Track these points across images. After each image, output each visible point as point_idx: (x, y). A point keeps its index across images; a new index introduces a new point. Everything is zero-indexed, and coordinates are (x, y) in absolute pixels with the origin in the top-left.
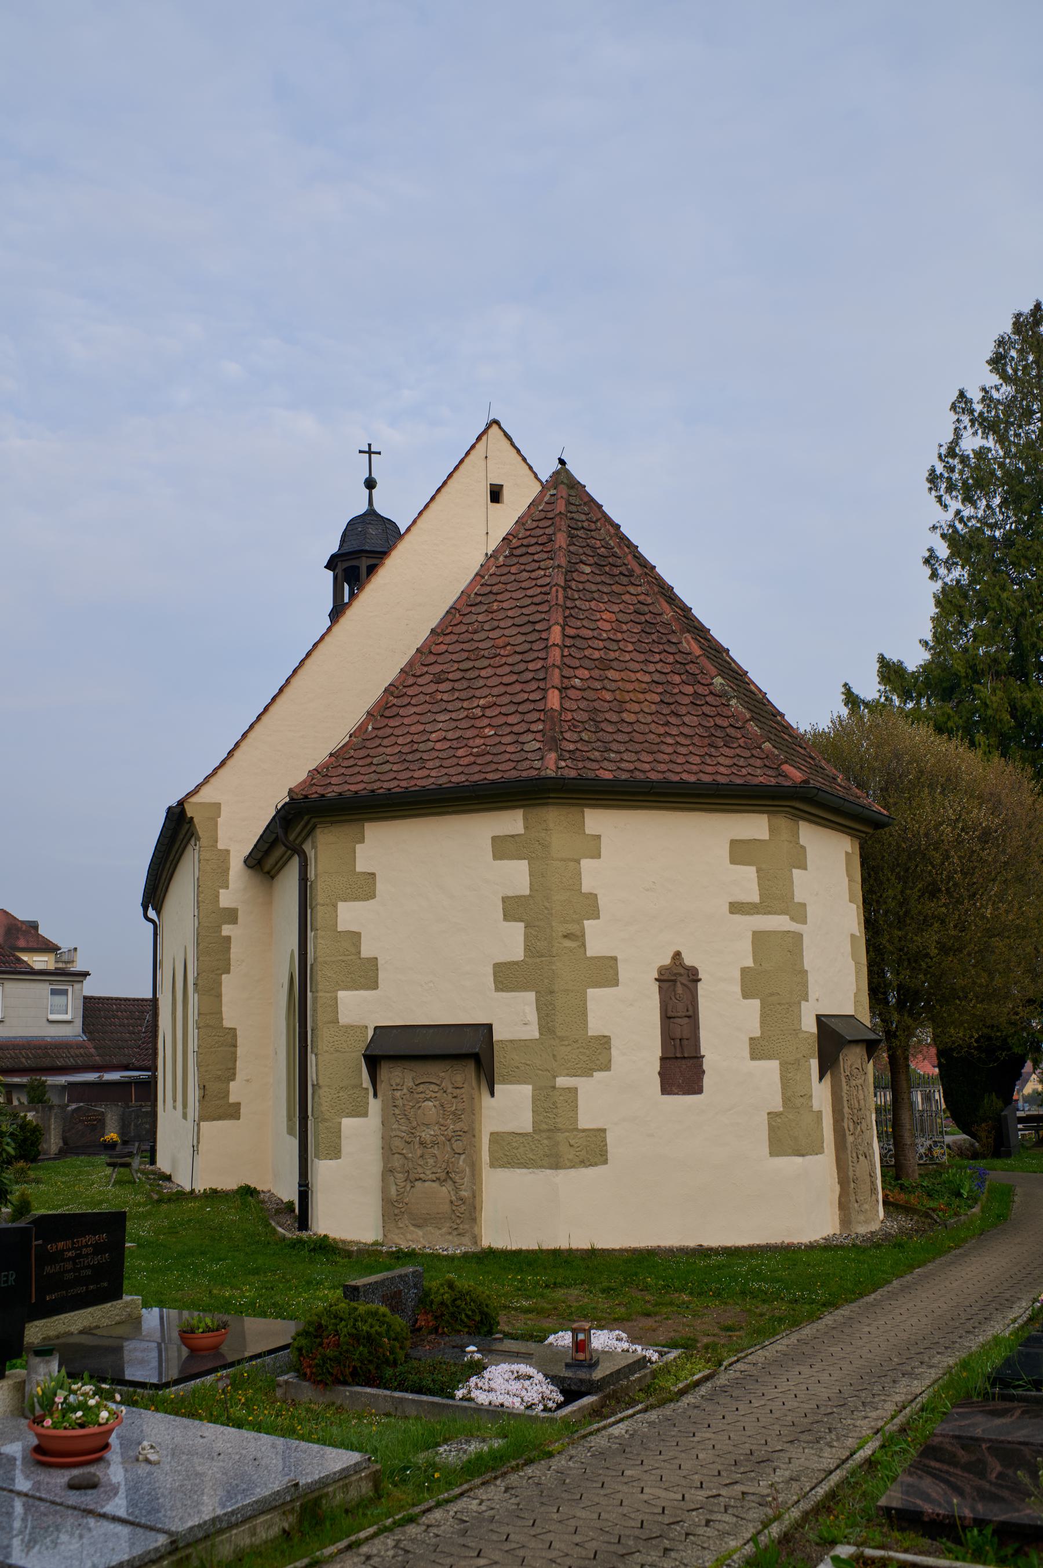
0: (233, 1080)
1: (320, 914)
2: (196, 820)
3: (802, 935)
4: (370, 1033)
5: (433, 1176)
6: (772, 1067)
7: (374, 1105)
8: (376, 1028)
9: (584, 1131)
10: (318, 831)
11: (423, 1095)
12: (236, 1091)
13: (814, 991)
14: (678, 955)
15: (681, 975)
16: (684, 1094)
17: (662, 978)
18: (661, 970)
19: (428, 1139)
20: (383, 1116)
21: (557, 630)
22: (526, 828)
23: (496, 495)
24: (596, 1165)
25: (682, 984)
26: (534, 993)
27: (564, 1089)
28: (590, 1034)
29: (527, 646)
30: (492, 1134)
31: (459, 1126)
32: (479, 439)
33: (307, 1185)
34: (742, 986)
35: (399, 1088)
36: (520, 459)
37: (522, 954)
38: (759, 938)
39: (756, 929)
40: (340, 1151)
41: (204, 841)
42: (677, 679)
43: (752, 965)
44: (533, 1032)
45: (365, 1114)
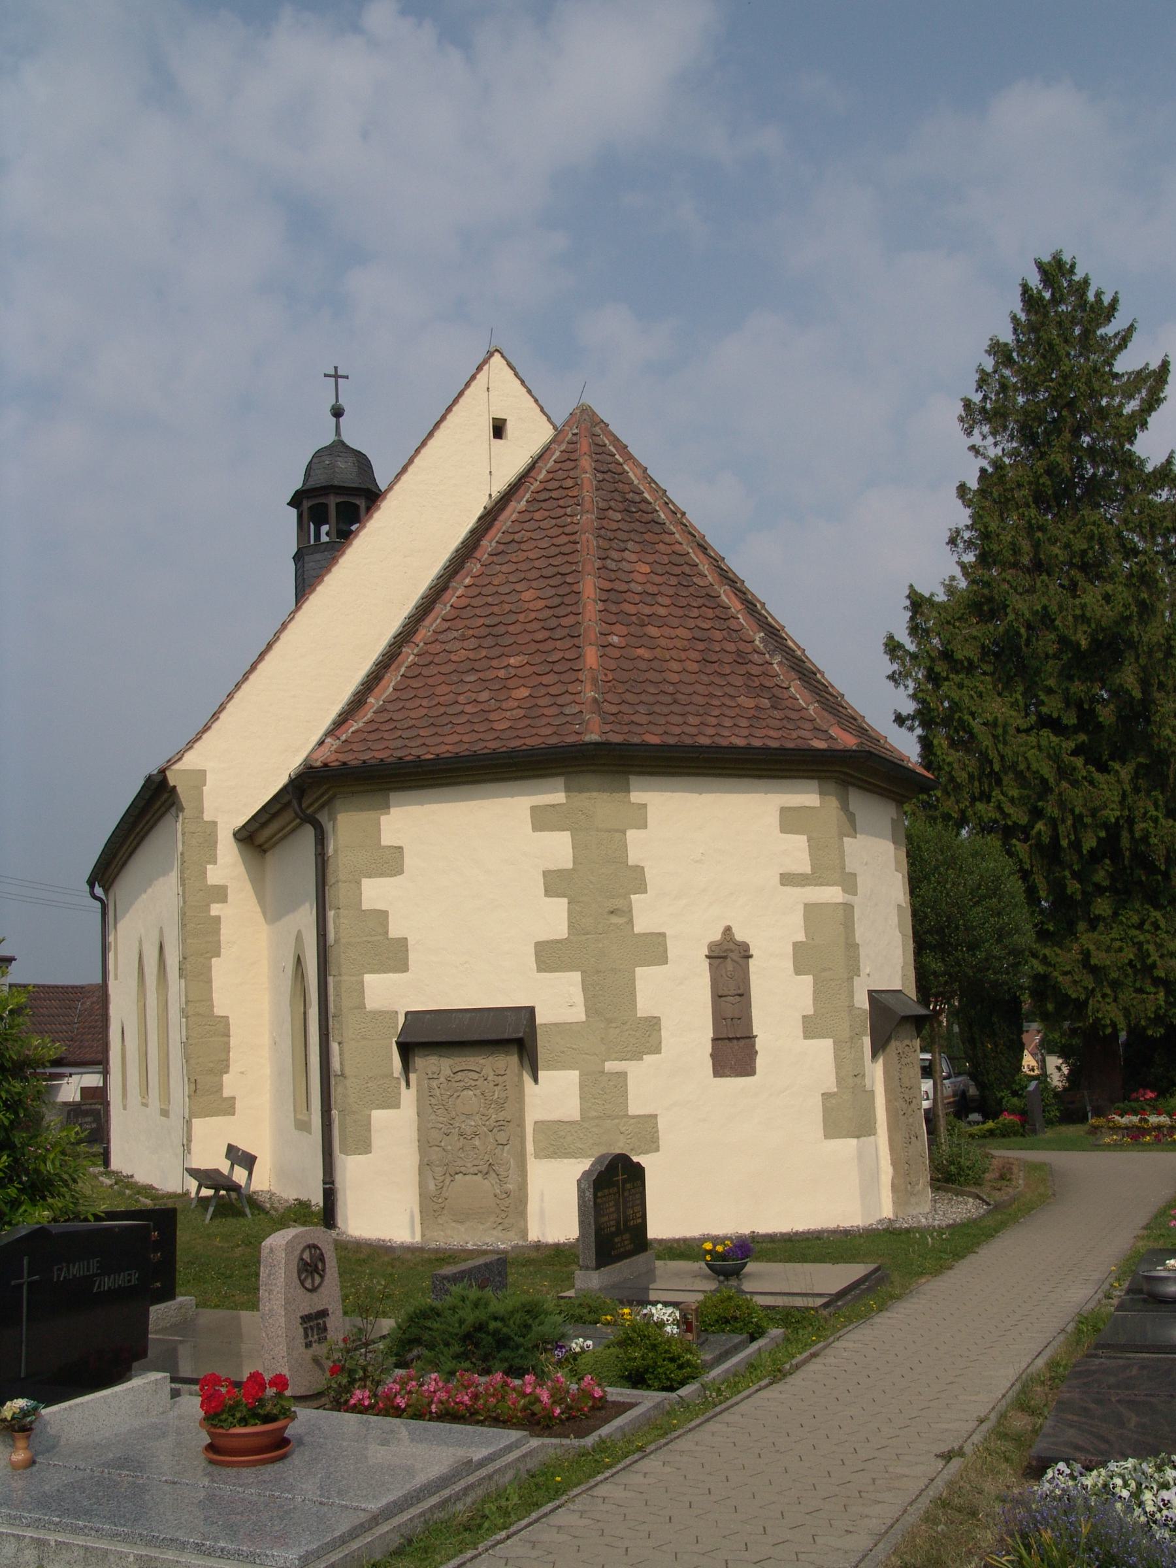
0: (227, 1072)
1: (339, 893)
2: (179, 790)
3: (853, 907)
4: (401, 1020)
5: (475, 1170)
6: (825, 1046)
7: (408, 1097)
8: (407, 1014)
9: (634, 1117)
10: (338, 803)
11: (462, 1084)
12: (230, 1084)
13: (866, 968)
14: (728, 930)
15: (732, 951)
16: (737, 1076)
18: (712, 946)
19: (469, 1131)
20: (418, 1108)
23: (498, 429)
25: (732, 960)
26: (579, 973)
27: (612, 1074)
29: (557, 601)
30: (536, 1123)
31: (502, 1115)
33: (332, 1183)
35: (435, 1076)
37: (566, 931)
38: (811, 910)
40: (370, 1145)
41: (188, 812)
42: (718, 635)
43: (804, 940)
44: (578, 1014)
45: (397, 1106)
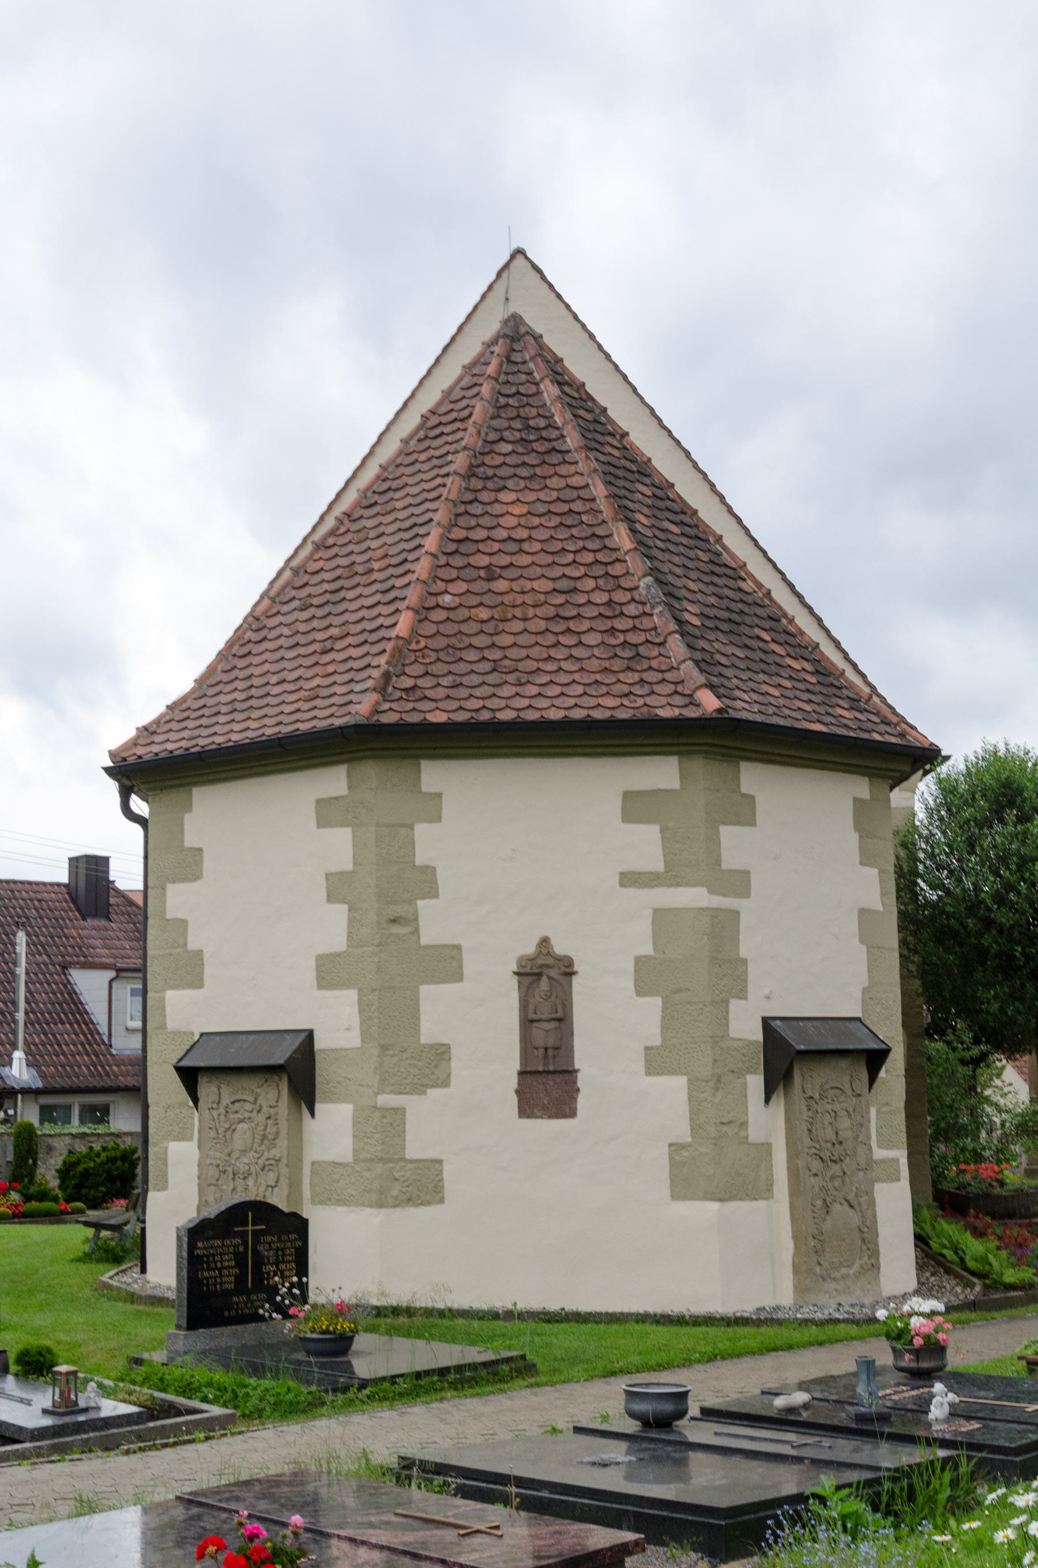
9: (412, 1161)
14: (545, 941)
15: (549, 967)
16: (550, 1117)
17: (522, 971)
18: (522, 961)
21: (435, 532)
22: (350, 788)
24: (428, 1203)
25: (549, 978)
28: (423, 1041)
32: (499, 274)
34: (636, 980)
36: (553, 295)
38: (661, 917)
39: (656, 906)
43: (652, 953)
